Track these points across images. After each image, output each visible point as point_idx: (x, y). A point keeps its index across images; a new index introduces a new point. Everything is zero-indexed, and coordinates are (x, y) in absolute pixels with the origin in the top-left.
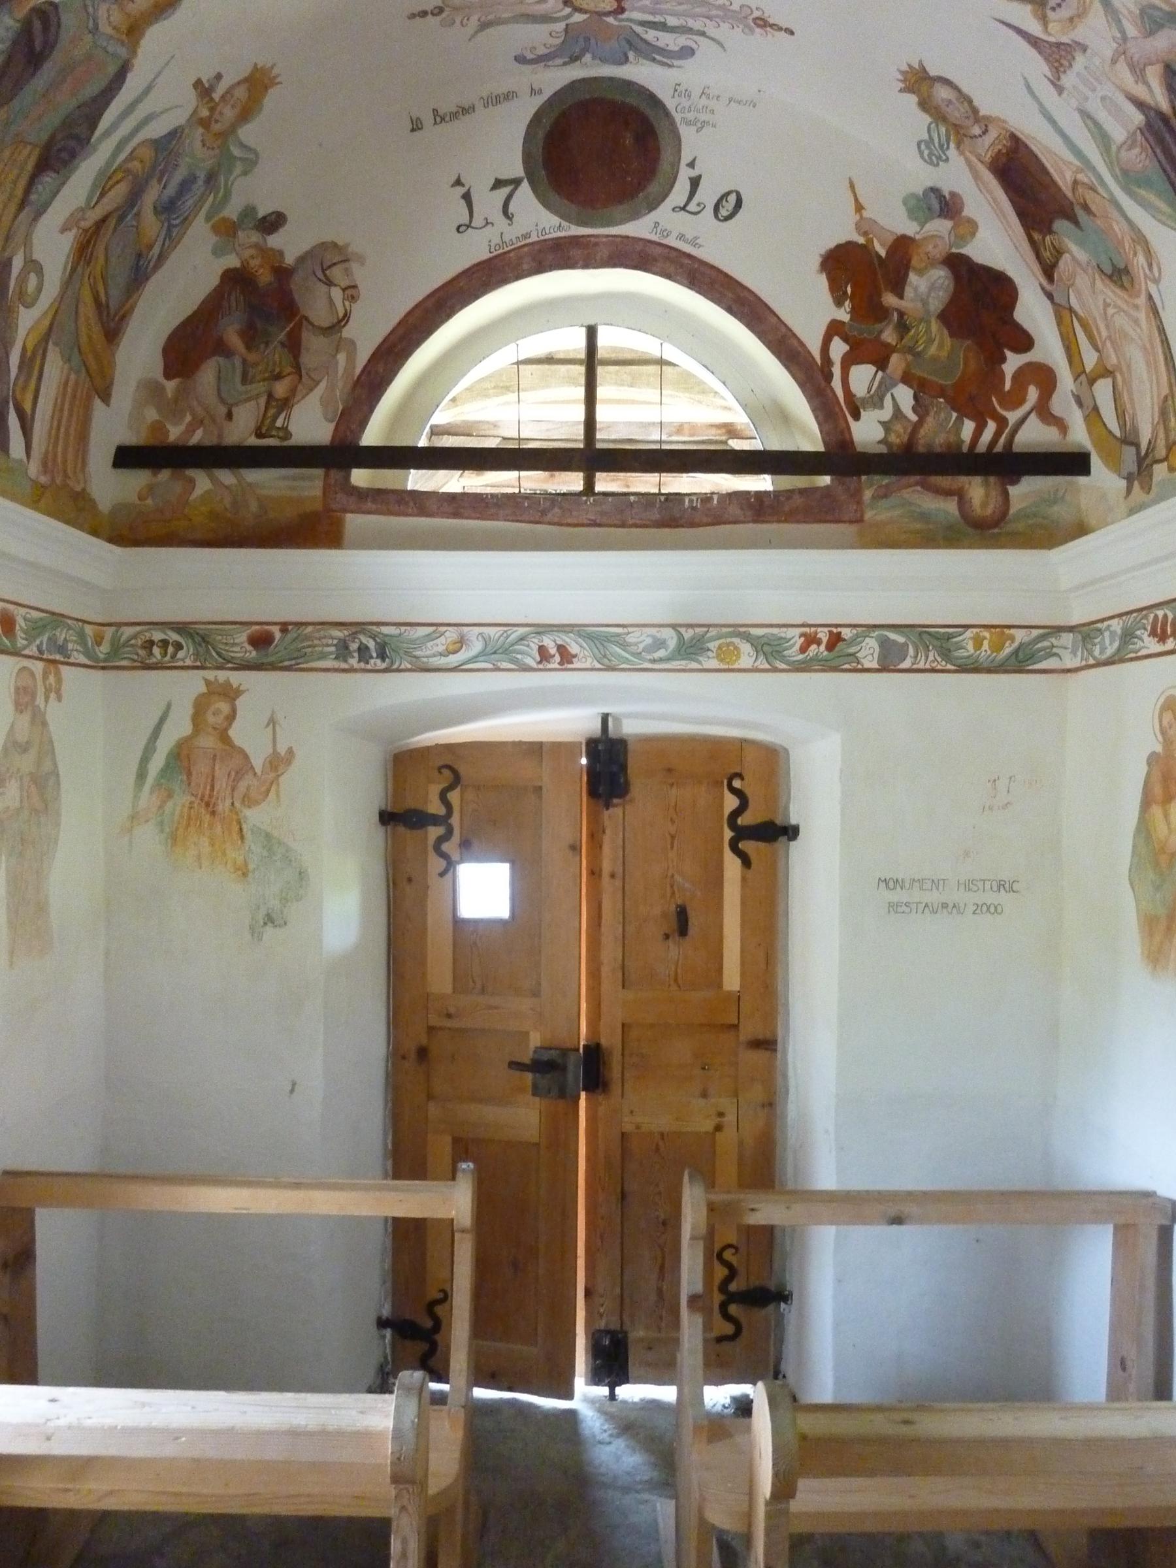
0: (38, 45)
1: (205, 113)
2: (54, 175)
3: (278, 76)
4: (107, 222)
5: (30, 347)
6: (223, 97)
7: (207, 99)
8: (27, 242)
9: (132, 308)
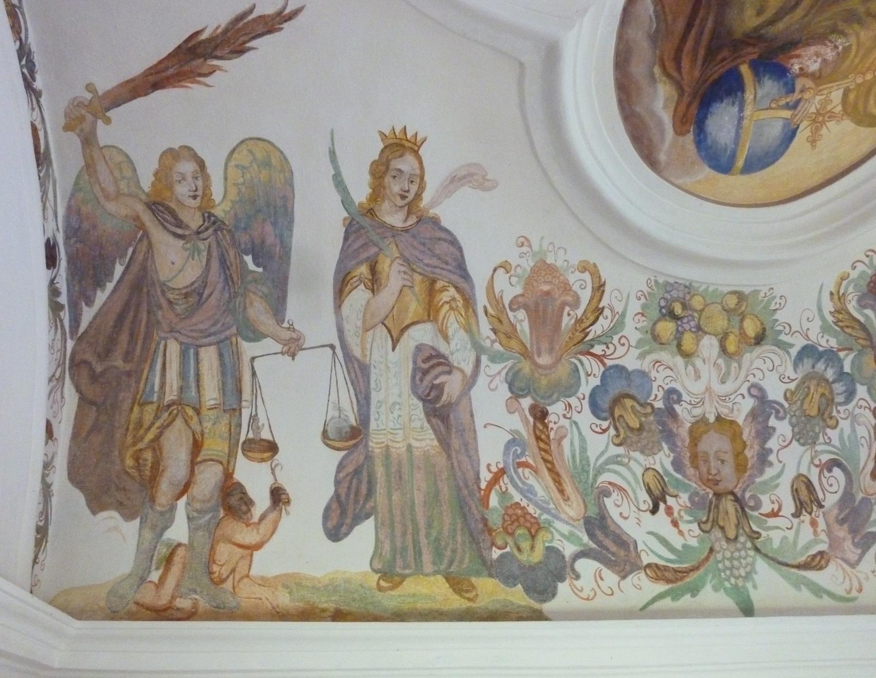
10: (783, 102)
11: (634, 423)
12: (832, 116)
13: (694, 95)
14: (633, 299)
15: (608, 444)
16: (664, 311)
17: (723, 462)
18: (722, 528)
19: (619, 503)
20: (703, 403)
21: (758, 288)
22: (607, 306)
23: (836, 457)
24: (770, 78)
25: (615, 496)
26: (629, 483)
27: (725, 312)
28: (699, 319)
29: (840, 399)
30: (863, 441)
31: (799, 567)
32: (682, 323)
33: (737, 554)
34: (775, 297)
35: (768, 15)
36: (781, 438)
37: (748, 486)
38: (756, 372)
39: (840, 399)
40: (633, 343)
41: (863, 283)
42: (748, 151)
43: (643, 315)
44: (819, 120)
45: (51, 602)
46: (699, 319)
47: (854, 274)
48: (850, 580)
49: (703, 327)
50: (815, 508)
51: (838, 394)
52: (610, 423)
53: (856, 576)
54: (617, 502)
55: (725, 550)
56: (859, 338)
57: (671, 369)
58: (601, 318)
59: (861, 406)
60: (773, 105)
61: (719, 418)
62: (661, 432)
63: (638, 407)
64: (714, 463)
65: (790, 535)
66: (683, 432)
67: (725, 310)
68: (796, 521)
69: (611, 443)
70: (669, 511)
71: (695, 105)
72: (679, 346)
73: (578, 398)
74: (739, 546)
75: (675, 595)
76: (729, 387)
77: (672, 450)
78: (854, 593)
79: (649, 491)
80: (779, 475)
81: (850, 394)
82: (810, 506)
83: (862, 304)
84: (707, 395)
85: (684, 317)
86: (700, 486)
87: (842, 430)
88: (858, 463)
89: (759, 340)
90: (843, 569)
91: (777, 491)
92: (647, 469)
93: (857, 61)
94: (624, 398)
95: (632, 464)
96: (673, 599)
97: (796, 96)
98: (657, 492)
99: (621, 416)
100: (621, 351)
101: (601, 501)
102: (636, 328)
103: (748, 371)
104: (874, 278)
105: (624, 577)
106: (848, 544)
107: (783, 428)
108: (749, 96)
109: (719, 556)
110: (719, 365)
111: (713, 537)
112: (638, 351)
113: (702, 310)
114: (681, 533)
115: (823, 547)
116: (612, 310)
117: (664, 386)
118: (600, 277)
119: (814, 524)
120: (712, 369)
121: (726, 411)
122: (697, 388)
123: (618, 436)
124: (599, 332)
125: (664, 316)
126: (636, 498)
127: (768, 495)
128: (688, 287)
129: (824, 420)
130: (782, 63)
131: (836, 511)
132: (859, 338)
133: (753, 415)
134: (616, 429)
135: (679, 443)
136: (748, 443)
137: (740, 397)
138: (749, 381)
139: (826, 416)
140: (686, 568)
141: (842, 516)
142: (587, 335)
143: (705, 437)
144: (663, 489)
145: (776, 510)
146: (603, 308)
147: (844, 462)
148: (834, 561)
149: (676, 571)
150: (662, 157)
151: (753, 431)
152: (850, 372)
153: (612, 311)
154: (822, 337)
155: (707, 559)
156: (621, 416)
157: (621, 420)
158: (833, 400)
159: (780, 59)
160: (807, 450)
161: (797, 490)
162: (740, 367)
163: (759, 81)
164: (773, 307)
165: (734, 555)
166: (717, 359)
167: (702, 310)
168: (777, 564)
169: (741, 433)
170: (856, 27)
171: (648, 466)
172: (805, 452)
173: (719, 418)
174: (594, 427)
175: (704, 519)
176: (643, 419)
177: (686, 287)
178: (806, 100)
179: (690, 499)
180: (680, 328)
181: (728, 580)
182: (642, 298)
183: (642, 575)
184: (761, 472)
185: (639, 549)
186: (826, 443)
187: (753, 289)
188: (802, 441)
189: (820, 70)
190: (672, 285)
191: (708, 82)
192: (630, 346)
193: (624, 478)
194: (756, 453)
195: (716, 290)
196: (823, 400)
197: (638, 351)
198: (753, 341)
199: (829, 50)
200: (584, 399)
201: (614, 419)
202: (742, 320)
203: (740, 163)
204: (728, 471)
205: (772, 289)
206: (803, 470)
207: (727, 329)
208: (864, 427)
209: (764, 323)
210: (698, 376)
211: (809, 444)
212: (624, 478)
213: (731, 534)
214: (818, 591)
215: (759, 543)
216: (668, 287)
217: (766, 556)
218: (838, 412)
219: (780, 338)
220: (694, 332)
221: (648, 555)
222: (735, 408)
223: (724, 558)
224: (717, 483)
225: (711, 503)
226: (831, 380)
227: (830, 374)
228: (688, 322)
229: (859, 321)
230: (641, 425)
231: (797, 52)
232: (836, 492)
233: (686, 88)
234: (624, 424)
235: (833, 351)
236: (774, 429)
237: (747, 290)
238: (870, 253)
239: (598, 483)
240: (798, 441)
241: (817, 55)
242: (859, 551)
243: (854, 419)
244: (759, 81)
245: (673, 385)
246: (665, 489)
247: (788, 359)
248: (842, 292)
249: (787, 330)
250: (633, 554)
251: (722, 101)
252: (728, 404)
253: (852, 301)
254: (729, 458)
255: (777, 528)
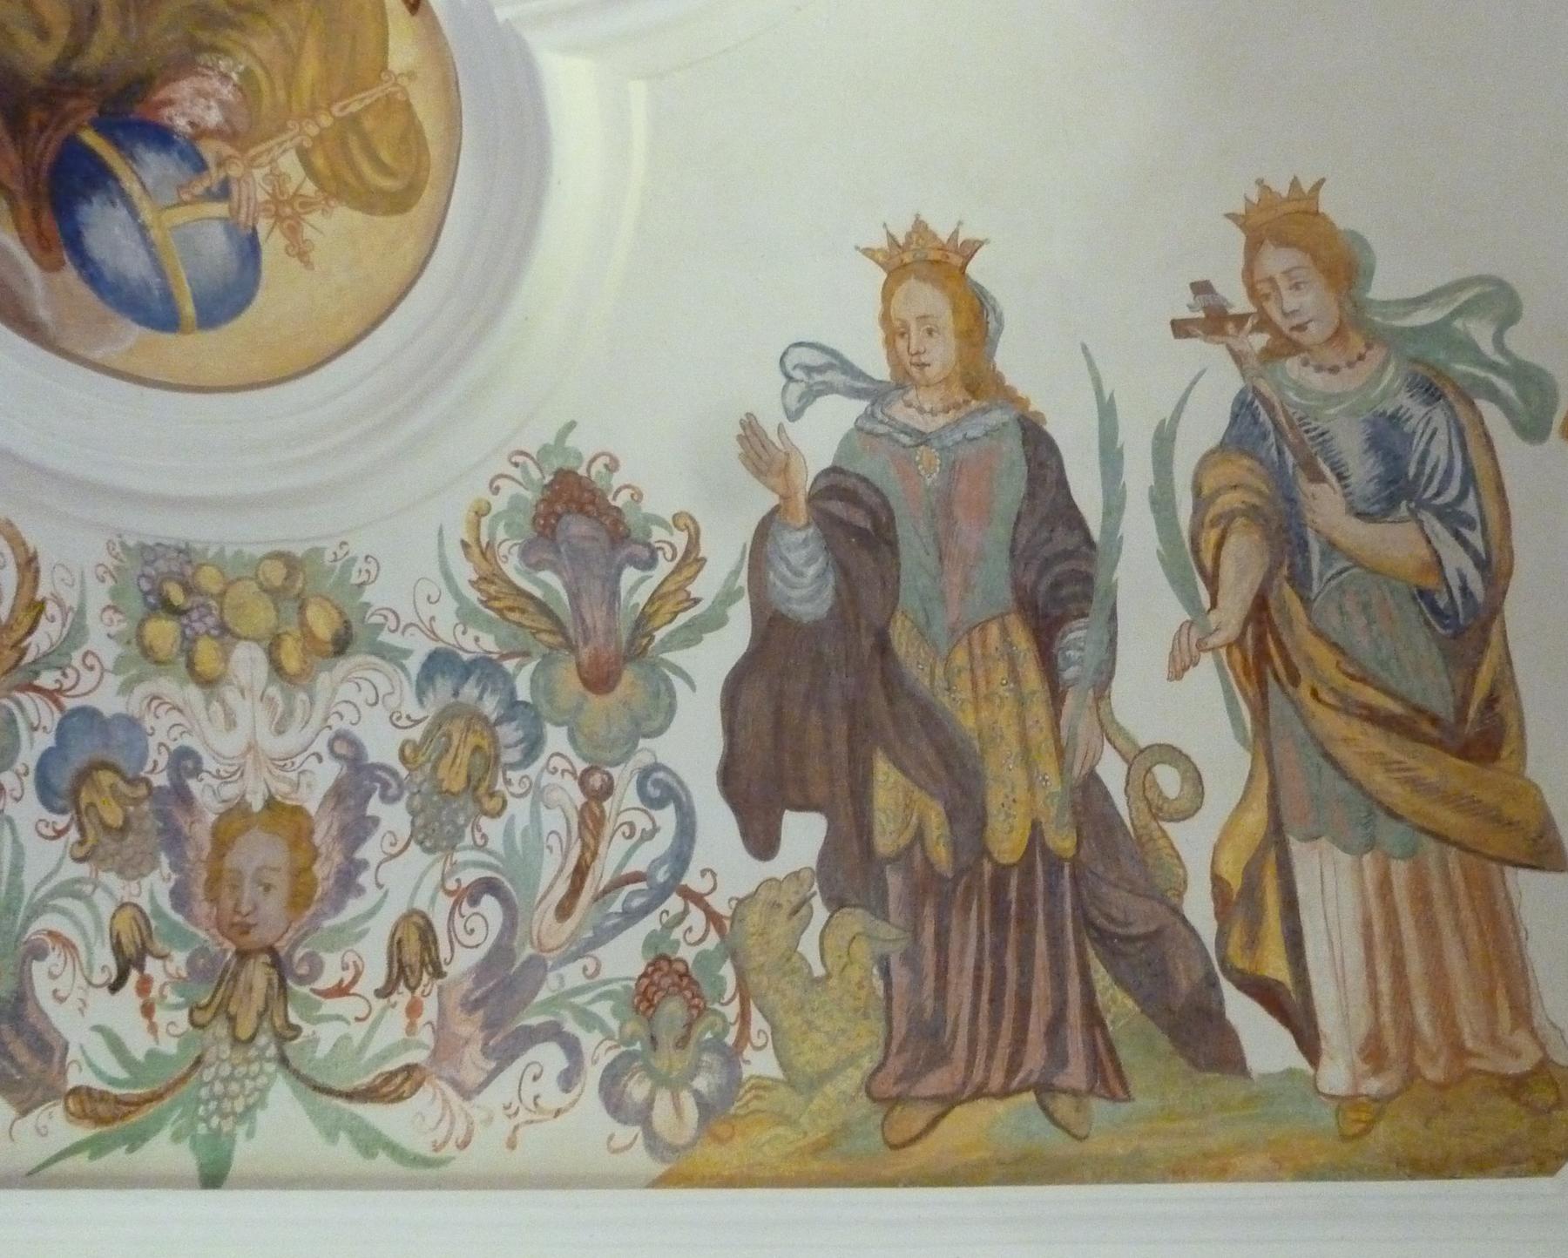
0: (860, 519)
1: (1260, 341)
2: (1082, 622)
3: (1295, 184)
4: (1272, 603)
5: (1234, 878)
6: (1253, 293)
7: (1230, 327)
8: (1108, 730)
9: (1505, 678)
10: (199, 189)
11: (114, 816)
12: (308, 205)
13: (33, 194)
14: (91, 582)
15: (62, 859)
16: (151, 599)
17: (268, 888)
18: (232, 1019)
19: (56, 971)
20: (242, 775)
21: (319, 544)
22: (48, 596)
23: (489, 874)
24: (147, 145)
25: (54, 958)
26: (84, 934)
27: (265, 596)
28: (222, 611)
29: (511, 756)
30: (553, 841)
31: (350, 1096)
32: (191, 621)
33: (242, 1070)
34: (354, 560)
35: (61, 34)
36: (389, 838)
37: (306, 934)
38: (342, 708)
39: (511, 756)
40: (109, 663)
41: (524, 520)
42: (190, 285)
43: (116, 610)
44: (290, 213)
45: (647, 1187)
46: (222, 611)
47: (499, 503)
48: (452, 1123)
49: (231, 626)
50: (425, 977)
51: (508, 747)
52: (72, 819)
53: (467, 1115)
54: (53, 969)
55: (223, 1061)
56: (539, 631)
57: (180, 711)
58: (43, 621)
59: (556, 770)
60: (186, 197)
61: (271, 803)
62: (161, 832)
63: (122, 786)
64: (249, 892)
65: (358, 1032)
66: (201, 832)
67: (266, 591)
68: (379, 1004)
69: (68, 855)
70: (144, 985)
71: (46, 216)
72: (190, 665)
73: (18, 775)
74: (253, 1053)
75: (96, 1147)
76: (292, 740)
77: (175, 867)
78: (450, 1150)
79: (117, 948)
80: (371, 913)
81: (533, 746)
82: (417, 974)
83: (533, 565)
84: (250, 757)
85: (191, 609)
86: (213, 937)
87: (512, 818)
88: (536, 885)
89: (342, 644)
90: (446, 1101)
91: (361, 947)
92: (123, 906)
93: (281, 95)
94: (97, 769)
95: (100, 898)
96: (92, 1157)
97: (214, 176)
98: (130, 950)
99: (92, 805)
100: (89, 679)
101: (26, 968)
102: (109, 635)
103: (328, 708)
104: (542, 507)
105: (24, 1113)
106: (473, 1052)
107: (393, 818)
108: (131, 185)
109: (208, 1075)
110: (272, 700)
111: (208, 1035)
112: (121, 679)
113: (223, 594)
114: (153, 1028)
115: (418, 1056)
116: (60, 604)
117: (168, 743)
118: (24, 544)
119: (414, 1010)
120: (259, 706)
121: (284, 788)
122: (231, 744)
123: (81, 843)
124: (45, 647)
125: (153, 608)
126: (90, 963)
127: (340, 954)
128: (185, 552)
129: (477, 801)
130: (150, 118)
131: (467, 984)
132: (539, 631)
133: (338, 794)
134: (82, 829)
135: (191, 854)
136: (323, 850)
137: (313, 759)
138: (330, 727)
139: (482, 791)
140: (139, 1096)
141: (478, 994)
142: (23, 653)
143: (241, 840)
144: (143, 944)
145: (346, 982)
146: (43, 603)
147: (508, 885)
148: (435, 1087)
149: (118, 1101)
150: (44, 313)
151: (335, 826)
152: (529, 700)
153: (59, 606)
154: (464, 633)
155: (183, 1079)
156: (92, 805)
157: (92, 814)
158: (497, 757)
159: (138, 112)
160: (437, 860)
161: (399, 942)
162: (312, 703)
163: (132, 156)
164: (355, 579)
165: (236, 1072)
166: (267, 686)
167: (223, 594)
168: (310, 1091)
169: (312, 832)
170: (234, 34)
171: (126, 900)
172: (432, 865)
173: (271, 803)
174: (42, 826)
175: (205, 1001)
176: (131, 808)
177: (180, 551)
178: (239, 180)
179: (190, 962)
180: (188, 632)
181: (206, 1120)
182: (108, 578)
183: (58, 1110)
184: (338, 907)
185: (69, 1058)
186: (477, 847)
187: (308, 546)
188: (428, 844)
189: (227, 121)
190: (152, 549)
191: (44, 175)
192: (103, 670)
193: (77, 923)
194: (334, 870)
195: (238, 554)
196: (478, 760)
197: (121, 679)
198: (330, 648)
199: (216, 83)
200: (26, 774)
201: (78, 812)
202: (302, 609)
203: (189, 309)
204: (273, 907)
205: (344, 543)
206: (421, 904)
207: (278, 628)
208: (558, 811)
209: (346, 610)
210: (231, 723)
211: (442, 850)
212: (77, 923)
213: (244, 1032)
214: (370, 1142)
215: (291, 1049)
216: (147, 553)
217: (297, 1074)
218: (508, 782)
219: (380, 638)
220: (215, 638)
221: (81, 1070)
222: (304, 780)
223: (216, 1077)
224: (246, 929)
225: (225, 971)
226: (493, 717)
227: (490, 706)
228: (200, 619)
229: (531, 597)
230: (127, 820)
231: (162, 94)
232: (477, 946)
233: (13, 187)
234: (96, 821)
235: (490, 660)
236: (376, 821)
237: (299, 551)
238: (520, 459)
239: (29, 933)
240: (421, 843)
241: (200, 93)
242: (492, 1065)
243: (537, 793)
244: (132, 156)
245: (187, 741)
246: (148, 945)
247: (406, 683)
248: (484, 540)
249: (392, 623)
250: (56, 1066)
251: (90, 202)
252: (289, 775)
253: (510, 557)
254: (281, 883)
255: (339, 1018)
